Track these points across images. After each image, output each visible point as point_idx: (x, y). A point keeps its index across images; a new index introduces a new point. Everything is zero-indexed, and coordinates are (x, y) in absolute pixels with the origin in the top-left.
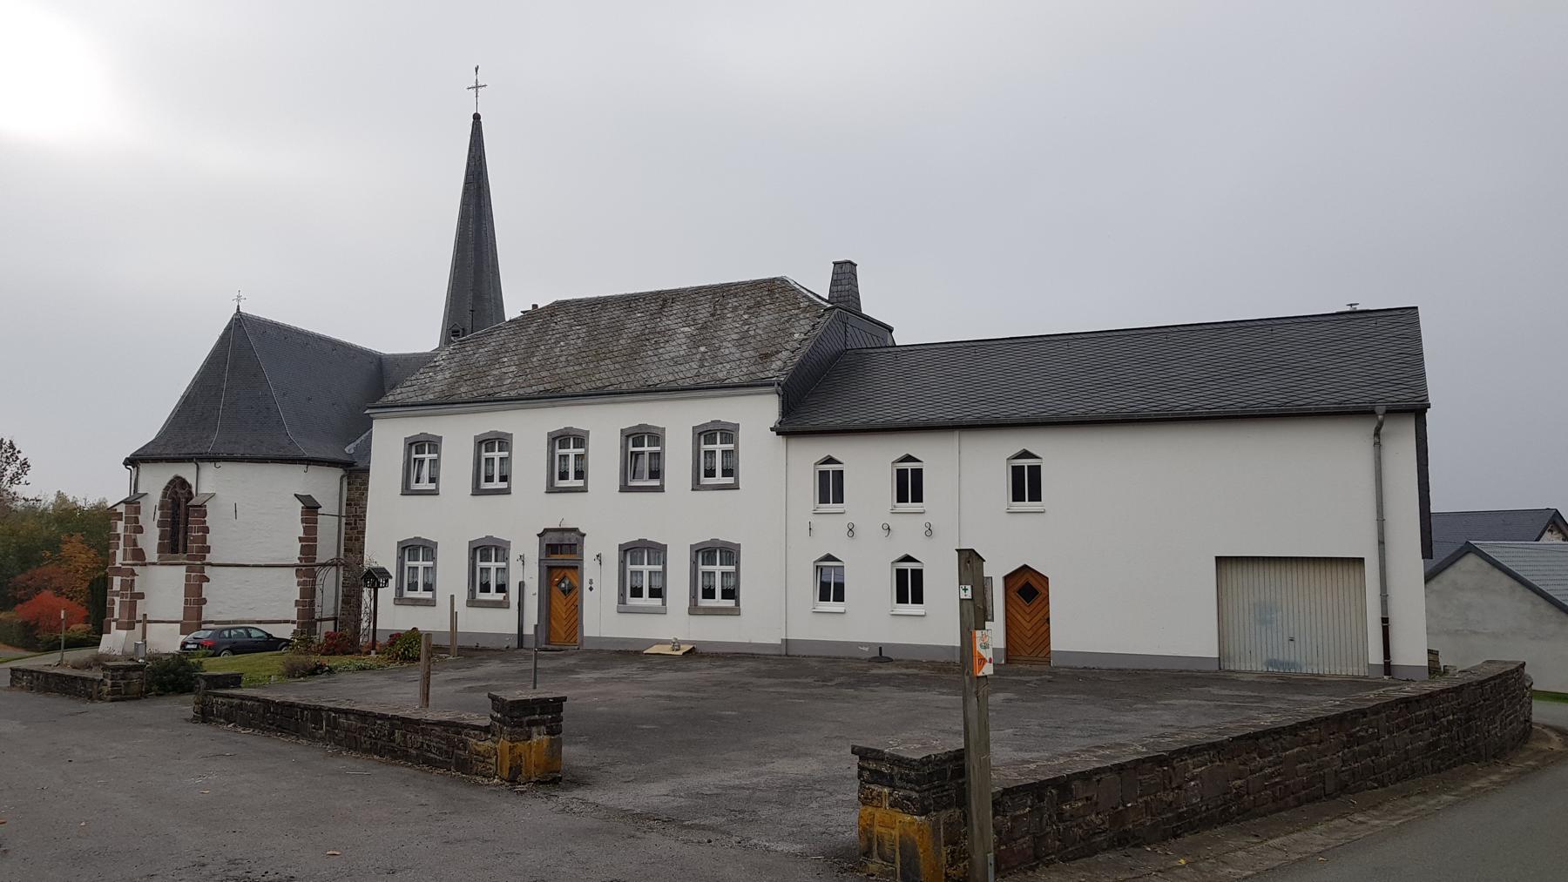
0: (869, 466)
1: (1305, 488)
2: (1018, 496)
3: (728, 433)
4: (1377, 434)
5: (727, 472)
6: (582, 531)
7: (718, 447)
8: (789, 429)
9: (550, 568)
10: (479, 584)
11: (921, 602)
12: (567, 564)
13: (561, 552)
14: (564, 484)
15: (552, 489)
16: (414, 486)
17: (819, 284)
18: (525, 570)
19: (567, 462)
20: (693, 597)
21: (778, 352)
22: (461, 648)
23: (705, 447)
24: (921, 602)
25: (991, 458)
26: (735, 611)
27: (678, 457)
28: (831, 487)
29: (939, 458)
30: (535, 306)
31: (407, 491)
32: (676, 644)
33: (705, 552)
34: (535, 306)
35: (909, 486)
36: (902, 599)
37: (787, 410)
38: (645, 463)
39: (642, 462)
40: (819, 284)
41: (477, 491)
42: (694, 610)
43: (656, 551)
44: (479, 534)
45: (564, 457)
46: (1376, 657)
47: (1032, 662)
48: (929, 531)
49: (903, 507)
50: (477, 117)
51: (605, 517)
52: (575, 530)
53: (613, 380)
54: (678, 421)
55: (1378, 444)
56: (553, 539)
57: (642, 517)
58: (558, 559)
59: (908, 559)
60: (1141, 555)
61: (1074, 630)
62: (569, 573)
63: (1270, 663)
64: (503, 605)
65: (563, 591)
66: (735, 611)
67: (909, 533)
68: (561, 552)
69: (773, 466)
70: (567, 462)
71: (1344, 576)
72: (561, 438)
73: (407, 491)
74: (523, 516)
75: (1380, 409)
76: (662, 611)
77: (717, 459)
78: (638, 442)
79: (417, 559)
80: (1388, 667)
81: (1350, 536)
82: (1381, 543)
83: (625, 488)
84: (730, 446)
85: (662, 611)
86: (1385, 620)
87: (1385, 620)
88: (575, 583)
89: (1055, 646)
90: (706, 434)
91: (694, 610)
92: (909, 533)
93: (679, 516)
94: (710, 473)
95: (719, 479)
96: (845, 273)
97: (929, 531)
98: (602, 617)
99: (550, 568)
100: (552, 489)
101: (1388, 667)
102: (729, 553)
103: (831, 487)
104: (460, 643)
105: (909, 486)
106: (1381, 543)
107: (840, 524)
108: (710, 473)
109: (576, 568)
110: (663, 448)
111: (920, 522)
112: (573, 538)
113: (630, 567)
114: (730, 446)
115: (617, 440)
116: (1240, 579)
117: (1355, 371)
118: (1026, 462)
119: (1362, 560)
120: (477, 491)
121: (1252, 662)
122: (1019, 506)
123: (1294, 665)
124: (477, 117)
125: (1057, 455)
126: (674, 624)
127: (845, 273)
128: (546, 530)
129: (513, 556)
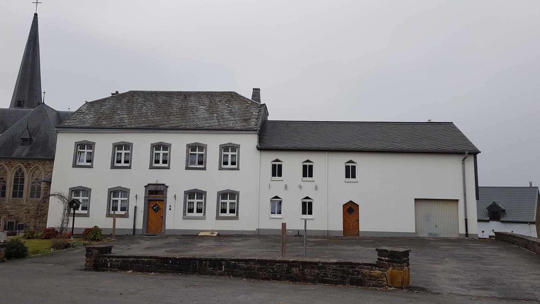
0: (292, 164)
1: (440, 177)
2: (347, 176)
3: (235, 148)
4: (463, 160)
5: (165, 162)
6: (167, 185)
7: (123, 152)
8: (262, 148)
9: (149, 200)
10: (112, 207)
11: (312, 214)
12: (158, 199)
13: (156, 195)
14: (157, 165)
15: (151, 167)
16: (78, 164)
17: (248, 95)
18: (137, 201)
19: (160, 157)
20: (217, 212)
21: (250, 119)
22: (116, 236)
23: (117, 151)
24: (312, 214)
25: (339, 162)
26: (236, 218)
27: (213, 156)
28: (277, 171)
29: (319, 162)
30: (117, 92)
31: (75, 166)
32: (212, 232)
33: (223, 195)
34: (117, 92)
35: (308, 171)
36: (304, 213)
37: (260, 140)
38: (85, 157)
39: (196, 158)
40: (248, 95)
41: (113, 167)
42: (218, 218)
43: (201, 194)
44: (223, 188)
45: (158, 154)
46: (462, 231)
47: (351, 235)
48: (316, 188)
49: (305, 179)
50: (36, 15)
51: (178, 180)
52: (163, 185)
53: (181, 124)
54: (213, 143)
55: (463, 164)
56: (152, 188)
57: (196, 180)
58: (154, 197)
59: (307, 198)
60: (389, 197)
61: (367, 224)
62: (158, 203)
63: (430, 234)
64: (126, 216)
65: (155, 210)
66: (236, 218)
67: (308, 188)
68: (156, 195)
69: (253, 161)
70: (160, 157)
71: (452, 206)
72: (193, 147)
73: (75, 166)
74: (138, 178)
75: (467, 152)
76: (203, 218)
77: (229, 158)
78: (194, 149)
79: (78, 196)
80: (467, 235)
81: (453, 192)
82: (465, 195)
83: (187, 168)
84: (91, 151)
85: (203, 218)
86: (466, 220)
87: (466, 220)
88: (160, 206)
89: (361, 229)
90: (225, 148)
91: (218, 218)
92: (308, 188)
93: (212, 180)
94: (226, 163)
95: (123, 164)
96: (256, 92)
97: (316, 188)
98: (175, 219)
99: (149, 200)
100: (151, 167)
101: (467, 235)
102: (233, 195)
103: (277, 171)
104: (116, 233)
105: (308, 171)
106: (465, 195)
107: (312, 185)
108: (226, 163)
109: (163, 201)
110: (94, 151)
111: (313, 184)
112: (162, 188)
113: (113, 199)
114: (91, 151)
115: (73, 146)
116: (422, 205)
117: (441, 141)
118: (308, 164)
119: (457, 201)
120: (113, 167)
121: (424, 234)
122: (348, 180)
123: (437, 234)
124: (36, 15)
125: (362, 162)
126: (209, 223)
127: (256, 92)
128: (149, 184)
129: (132, 195)
